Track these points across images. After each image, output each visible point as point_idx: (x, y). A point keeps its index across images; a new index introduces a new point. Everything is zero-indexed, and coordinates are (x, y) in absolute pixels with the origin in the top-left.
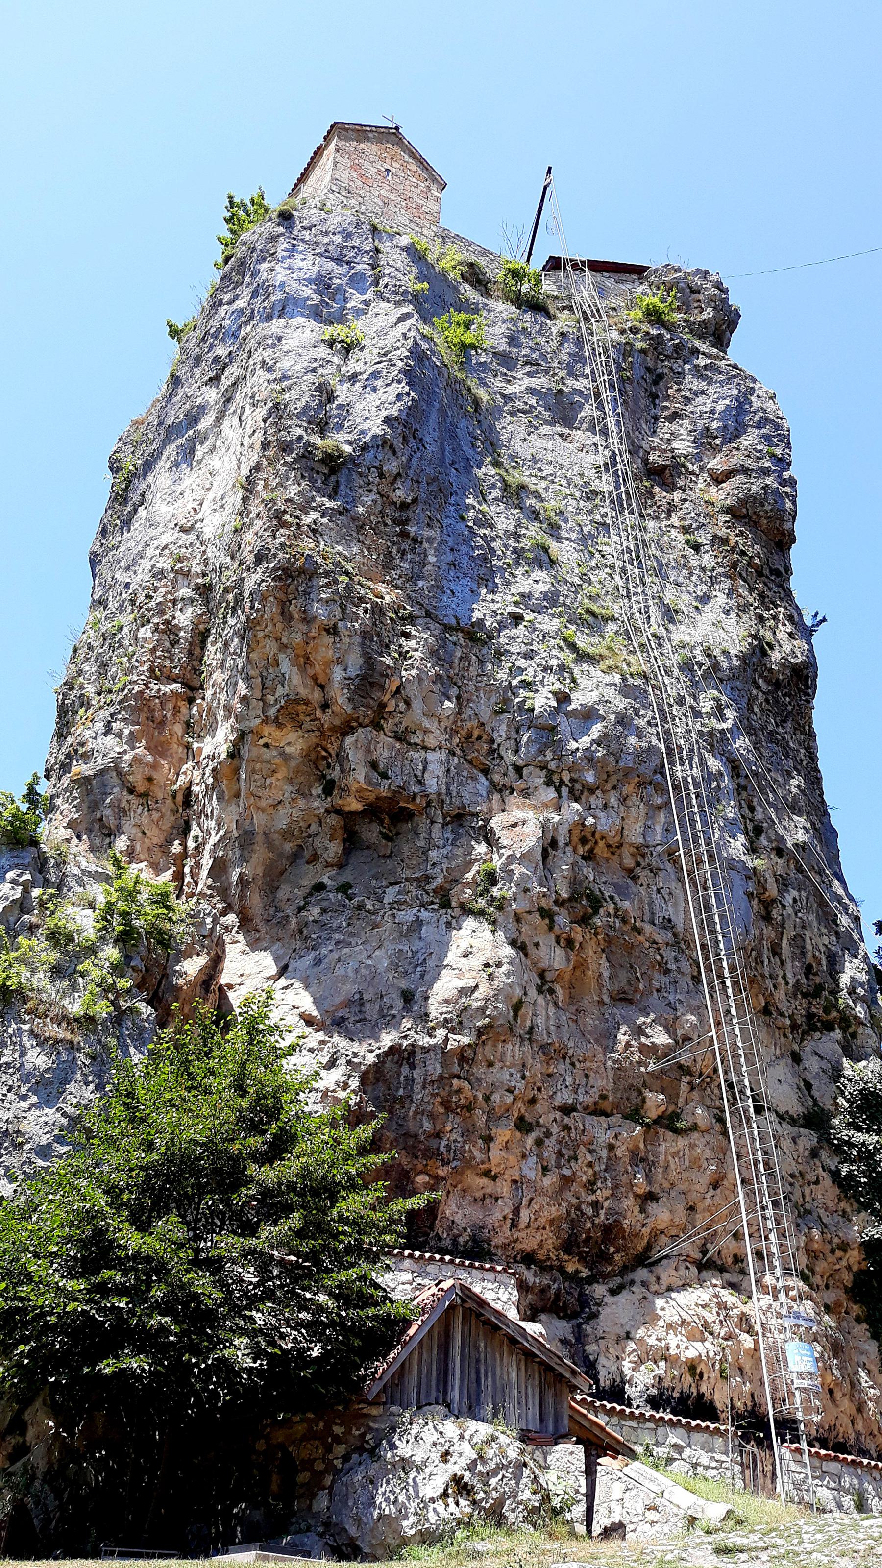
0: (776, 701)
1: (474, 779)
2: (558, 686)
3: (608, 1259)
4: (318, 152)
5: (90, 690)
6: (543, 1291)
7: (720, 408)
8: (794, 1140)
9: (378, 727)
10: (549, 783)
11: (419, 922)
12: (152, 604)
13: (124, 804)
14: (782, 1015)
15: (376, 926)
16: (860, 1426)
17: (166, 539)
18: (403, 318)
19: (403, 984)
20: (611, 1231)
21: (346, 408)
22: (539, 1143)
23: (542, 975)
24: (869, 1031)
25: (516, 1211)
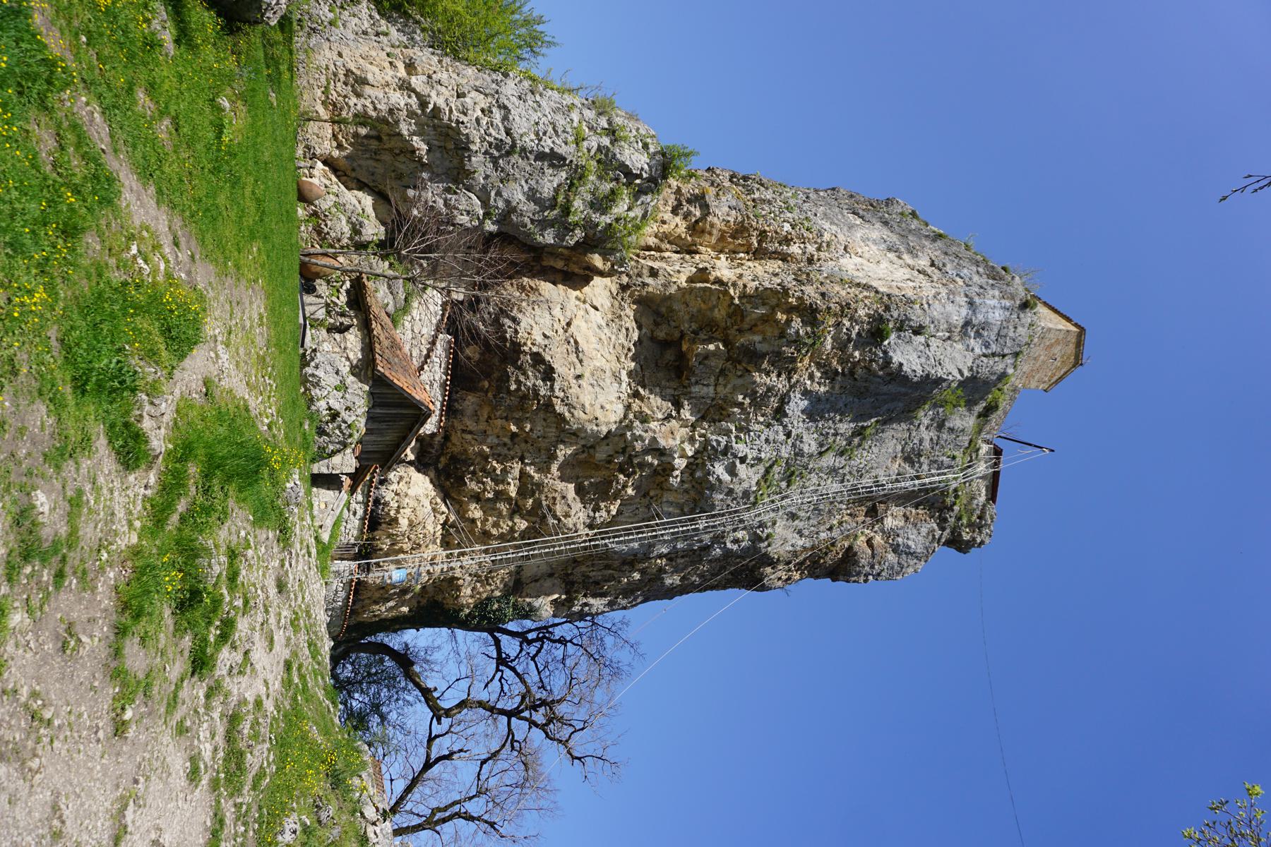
2: (750, 457)
3: (448, 478)
4: (1069, 320)
5: (757, 195)
7: (910, 543)
9: (727, 360)
12: (803, 231)
16: (367, 601)
17: (841, 237)
18: (960, 371)
19: (587, 374)
21: (910, 342)
22: (505, 444)
23: (592, 447)
25: (470, 432)
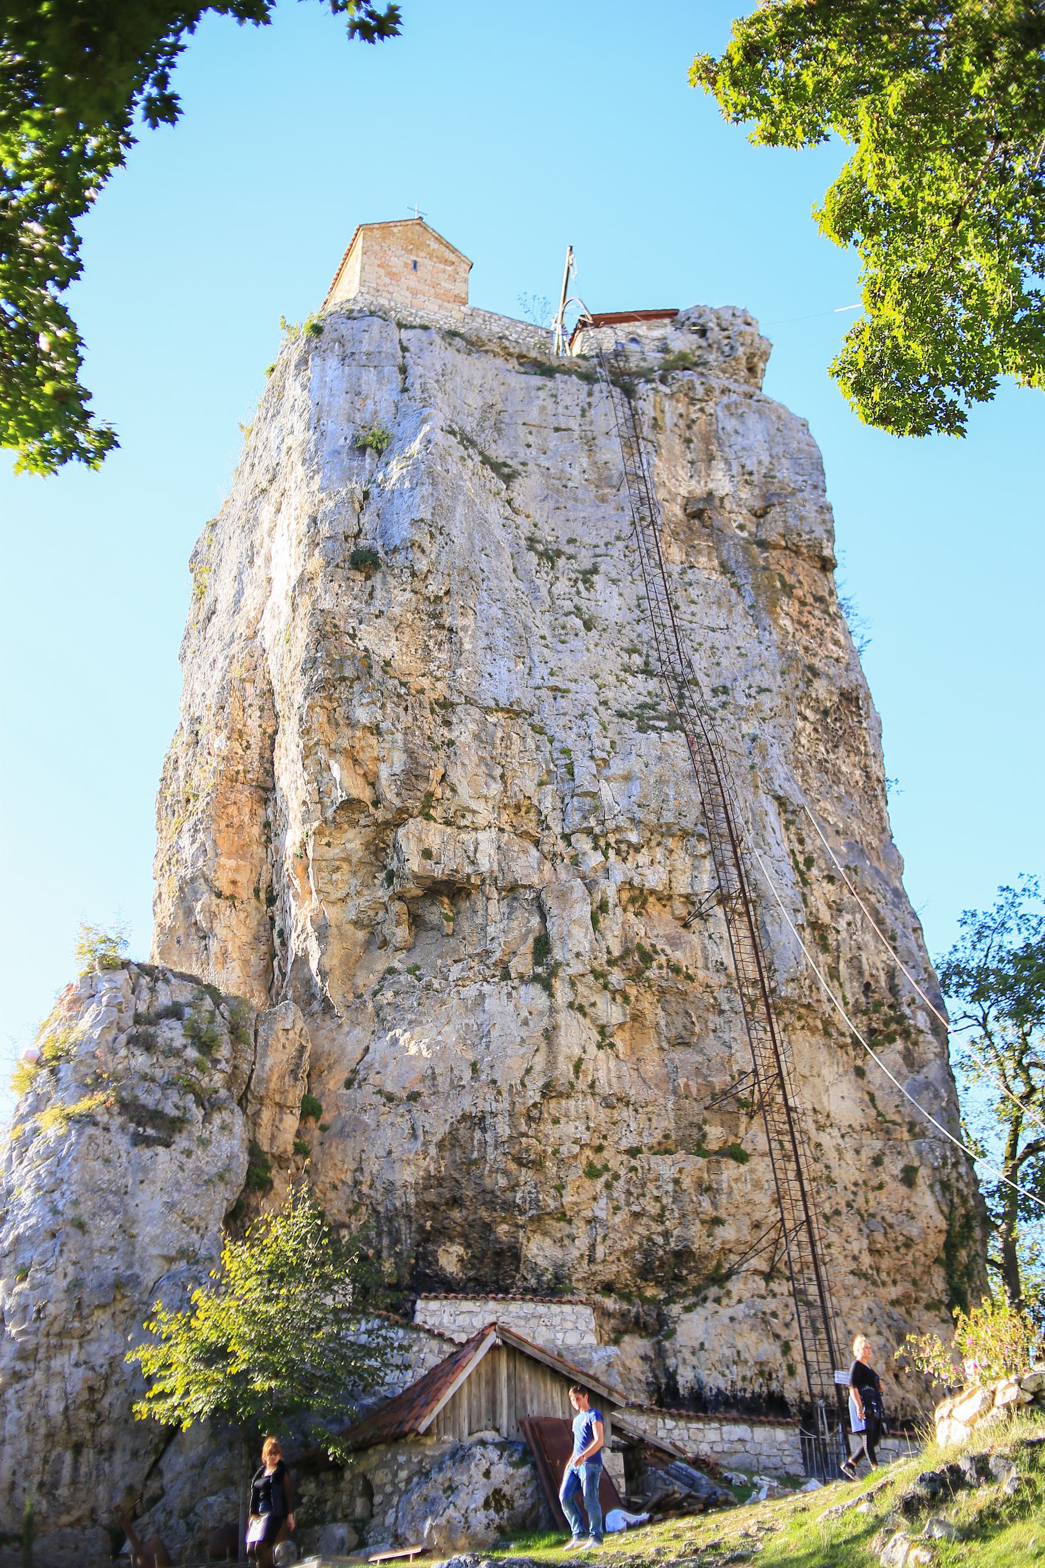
0: (826, 728)
1: (525, 852)
6: (624, 1315)
8: (857, 1152)
9: (428, 817)
10: (595, 848)
11: (482, 996)
13: (214, 908)
14: (843, 1034)
15: (443, 1003)
19: (470, 1056)
20: (683, 1255)
22: (608, 1186)
24: (930, 1037)
25: (593, 1247)
